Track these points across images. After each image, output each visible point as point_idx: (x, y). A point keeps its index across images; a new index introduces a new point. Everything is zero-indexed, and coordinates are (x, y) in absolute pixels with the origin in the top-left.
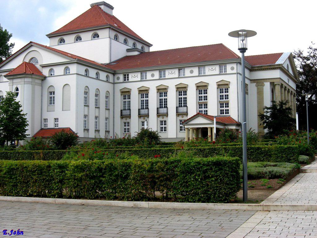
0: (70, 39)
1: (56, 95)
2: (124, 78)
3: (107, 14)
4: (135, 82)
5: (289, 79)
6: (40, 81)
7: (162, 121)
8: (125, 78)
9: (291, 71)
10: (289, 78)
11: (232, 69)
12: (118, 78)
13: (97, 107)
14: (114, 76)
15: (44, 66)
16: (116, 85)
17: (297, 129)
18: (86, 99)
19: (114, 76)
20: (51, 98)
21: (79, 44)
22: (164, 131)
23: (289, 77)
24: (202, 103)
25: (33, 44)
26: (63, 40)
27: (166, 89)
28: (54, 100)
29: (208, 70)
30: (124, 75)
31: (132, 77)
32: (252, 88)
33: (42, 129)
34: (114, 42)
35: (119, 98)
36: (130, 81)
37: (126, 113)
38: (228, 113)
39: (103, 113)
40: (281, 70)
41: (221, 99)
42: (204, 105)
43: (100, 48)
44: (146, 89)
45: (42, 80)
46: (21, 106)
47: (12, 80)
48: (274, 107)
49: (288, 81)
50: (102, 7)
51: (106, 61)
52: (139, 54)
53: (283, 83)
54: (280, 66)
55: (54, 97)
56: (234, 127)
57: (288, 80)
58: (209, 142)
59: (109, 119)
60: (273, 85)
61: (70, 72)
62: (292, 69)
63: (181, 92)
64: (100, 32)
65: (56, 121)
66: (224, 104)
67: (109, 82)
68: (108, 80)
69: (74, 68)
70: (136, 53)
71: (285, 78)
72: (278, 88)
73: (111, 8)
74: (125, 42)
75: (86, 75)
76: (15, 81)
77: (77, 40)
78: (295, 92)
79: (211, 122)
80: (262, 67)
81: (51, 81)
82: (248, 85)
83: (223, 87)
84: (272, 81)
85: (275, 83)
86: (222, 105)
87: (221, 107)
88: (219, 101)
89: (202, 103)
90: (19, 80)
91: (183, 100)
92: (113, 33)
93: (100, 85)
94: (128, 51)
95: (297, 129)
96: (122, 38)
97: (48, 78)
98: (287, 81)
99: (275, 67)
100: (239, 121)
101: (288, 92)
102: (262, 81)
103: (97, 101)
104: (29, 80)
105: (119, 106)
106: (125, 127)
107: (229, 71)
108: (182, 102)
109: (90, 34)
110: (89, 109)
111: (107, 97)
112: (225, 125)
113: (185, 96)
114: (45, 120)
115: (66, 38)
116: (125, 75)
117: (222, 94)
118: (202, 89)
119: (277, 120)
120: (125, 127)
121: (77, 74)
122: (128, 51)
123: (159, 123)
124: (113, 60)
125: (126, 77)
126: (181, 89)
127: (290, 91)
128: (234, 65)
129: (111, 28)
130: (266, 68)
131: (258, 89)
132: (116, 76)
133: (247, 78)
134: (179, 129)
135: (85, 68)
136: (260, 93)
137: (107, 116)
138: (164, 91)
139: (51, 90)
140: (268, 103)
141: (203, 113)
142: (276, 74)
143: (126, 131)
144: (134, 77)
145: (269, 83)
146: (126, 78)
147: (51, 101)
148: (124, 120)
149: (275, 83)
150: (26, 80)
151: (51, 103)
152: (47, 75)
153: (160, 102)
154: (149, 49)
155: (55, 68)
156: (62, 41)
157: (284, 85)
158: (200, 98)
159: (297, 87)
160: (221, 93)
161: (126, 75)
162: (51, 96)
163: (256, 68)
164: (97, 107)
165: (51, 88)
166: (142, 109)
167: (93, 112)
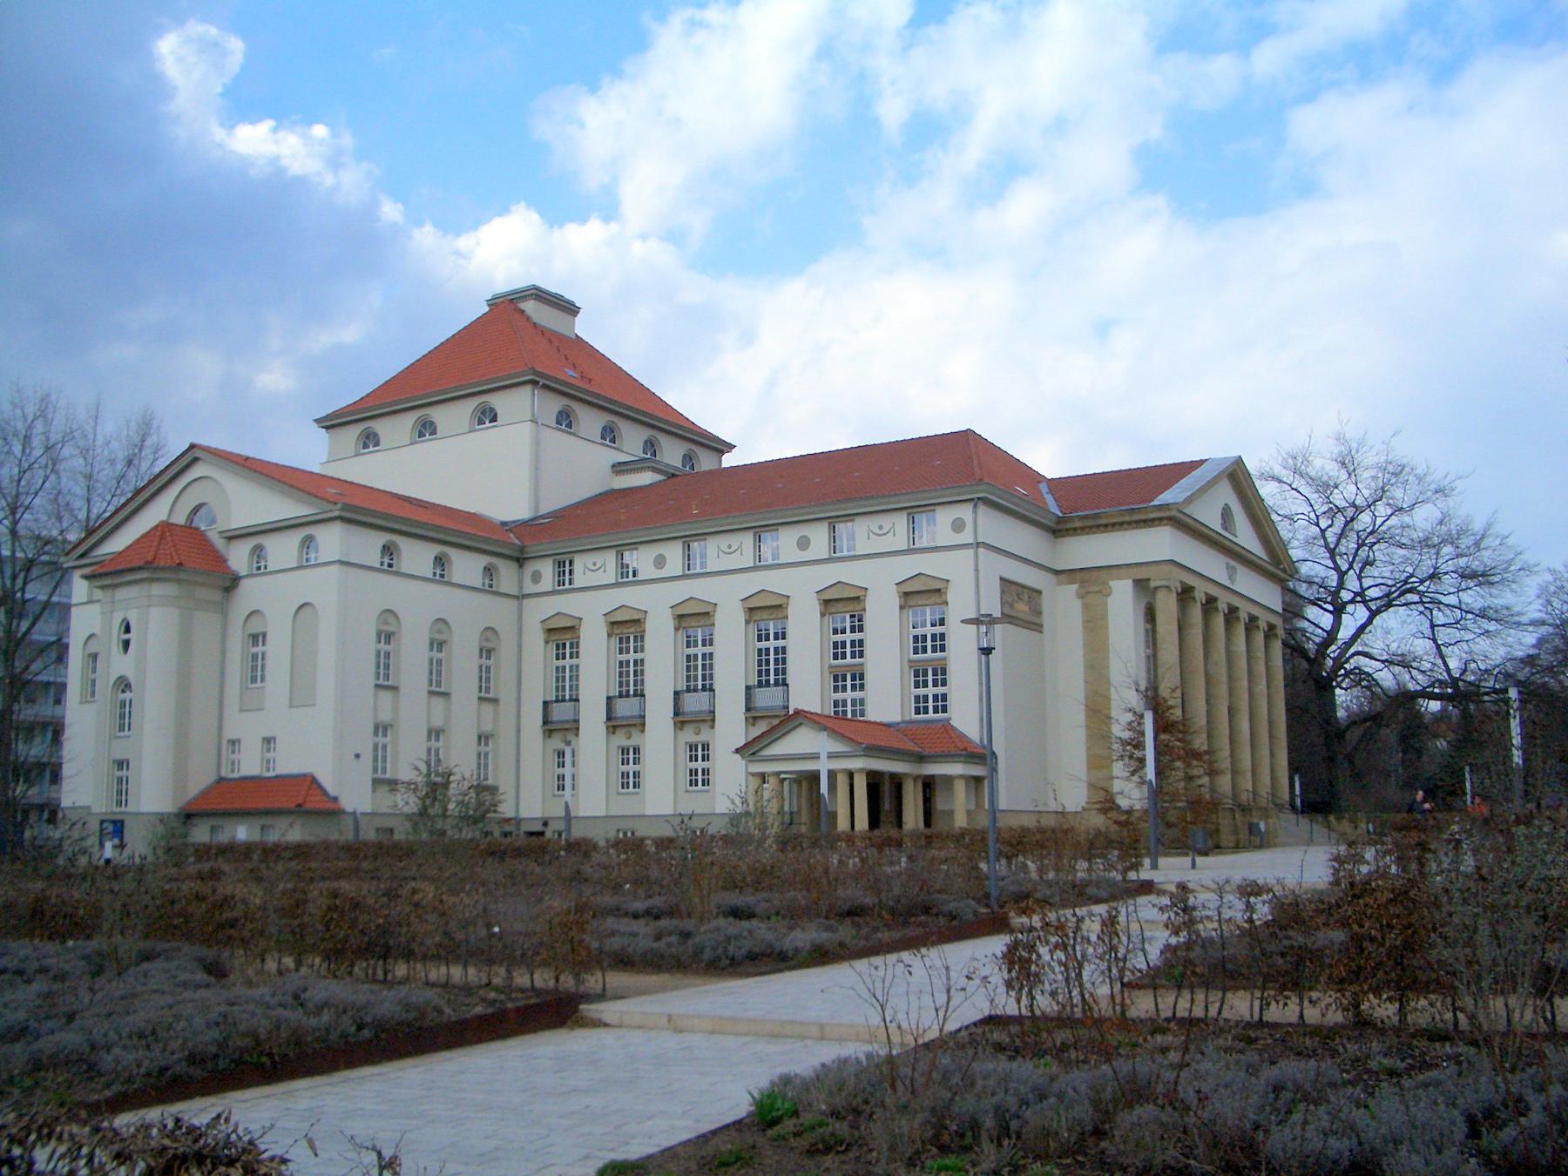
0: (396, 429)
3: (542, 331)
6: (216, 595)
10: (1232, 563)
12: (536, 578)
13: (438, 693)
14: (521, 566)
15: (233, 537)
16: (525, 602)
17: (1517, 757)
19: (521, 566)
21: (429, 447)
25: (197, 453)
26: (376, 435)
27: (707, 614)
29: (784, 543)
33: (221, 780)
35: (537, 649)
36: (577, 585)
37: (561, 712)
38: (944, 710)
41: (835, 658)
43: (496, 464)
44: (569, 624)
47: (109, 592)
49: (1231, 578)
50: (529, 307)
53: (1191, 581)
54: (1168, 514)
64: (499, 401)
65: (625, 762)
66: (928, 669)
69: (332, 540)
70: (646, 478)
72: (1167, 606)
73: (571, 309)
74: (609, 435)
77: (421, 435)
80: (1096, 516)
81: (252, 593)
82: (1039, 592)
84: (1142, 574)
85: (1153, 584)
88: (910, 661)
91: (772, 657)
92: (555, 404)
95: (1517, 757)
96: (590, 421)
97: (245, 584)
99: (1152, 516)
102: (1104, 573)
103: (436, 670)
104: (170, 589)
105: (537, 689)
108: (771, 668)
109: (467, 408)
111: (487, 652)
112: (921, 759)
114: (233, 742)
115: (381, 427)
116: (561, 564)
121: (341, 563)
123: (684, 753)
124: (545, 510)
125: (564, 568)
128: (965, 512)
131: (1086, 607)
132: (531, 567)
133: (51, 596)
134: (616, 780)
135: (382, 538)
136: (1095, 625)
139: (254, 626)
142: (1157, 544)
144: (594, 568)
145: (1129, 583)
148: (689, 735)
150: (157, 589)
152: (243, 572)
156: (370, 440)
158: (838, 650)
163: (1077, 524)
164: (438, 693)
165: (254, 619)
166: (760, 685)
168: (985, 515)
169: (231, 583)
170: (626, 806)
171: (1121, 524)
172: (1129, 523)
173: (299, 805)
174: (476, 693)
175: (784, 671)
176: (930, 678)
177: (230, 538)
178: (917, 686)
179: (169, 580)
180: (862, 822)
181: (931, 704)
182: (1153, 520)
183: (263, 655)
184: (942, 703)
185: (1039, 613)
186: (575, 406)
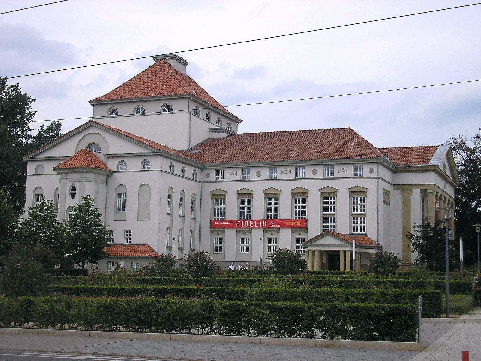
1: (128, 199)
2: (217, 175)
4: (232, 183)
5: (446, 183)
6: (104, 178)
7: (271, 238)
8: (217, 175)
9: (448, 173)
10: (445, 182)
11: (371, 171)
12: (208, 175)
14: (202, 171)
18: (170, 205)
20: (119, 201)
21: (141, 118)
22: (246, 252)
23: (446, 181)
24: (328, 216)
28: (124, 205)
30: (217, 171)
31: (228, 175)
32: (396, 196)
34: (194, 118)
35: (208, 202)
38: (364, 231)
39: (188, 225)
40: (435, 172)
42: (331, 218)
43: (178, 129)
45: (108, 176)
46: (101, 215)
47: (65, 175)
48: (425, 226)
50: (173, 62)
51: (184, 147)
52: (228, 137)
53: (438, 190)
54: (435, 168)
55: (125, 201)
56: (373, 251)
57: (445, 184)
58: (311, 273)
59: (194, 232)
60: (424, 194)
61: (151, 166)
62: (449, 167)
63: (299, 199)
65: (127, 235)
66: (358, 218)
67: (185, 177)
68: (194, 177)
70: (224, 135)
71: (440, 183)
73: (184, 63)
75: (171, 173)
76: (70, 176)
78: (453, 201)
79: (343, 243)
81: (120, 178)
83: (358, 196)
84: (424, 188)
85: (428, 191)
86: (355, 219)
87: (354, 222)
89: (328, 216)
90: (77, 176)
91: (301, 210)
92: (193, 106)
93: (184, 182)
94: (212, 131)
96: (203, 112)
97: (117, 175)
98: (442, 187)
99: (429, 169)
100: (380, 243)
101: (445, 201)
104: (92, 176)
106: (216, 245)
107: (366, 173)
110: (172, 219)
113: (304, 205)
116: (217, 171)
117: (356, 204)
118: (328, 196)
119: (431, 244)
120: (216, 245)
122: (212, 131)
125: (219, 174)
126: (299, 196)
127: (447, 200)
128: (374, 167)
129: (190, 98)
130: (416, 169)
132: (205, 172)
135: (170, 161)
137: (169, 225)
138: (274, 196)
139: (121, 190)
140: (417, 218)
141: (329, 230)
142: (430, 179)
143: (217, 250)
146: (219, 175)
147: (119, 205)
149: (428, 191)
150: (88, 175)
151: (119, 209)
152: (115, 170)
153: (268, 212)
154: (237, 126)
155: (128, 161)
156: (114, 112)
157: (440, 192)
159: (456, 191)
160: (354, 202)
161: (219, 171)
162: (120, 198)
165: (121, 187)
167: (177, 223)
168: (381, 168)
169: (110, 173)
170: (244, 258)
171: (417, 170)
172: (420, 170)
173: (151, 255)
174: (191, 217)
175: (305, 215)
176: (359, 220)
177: (108, 157)
178: (242, 204)
179: (93, 172)
180: (348, 268)
181: (359, 229)
182: (429, 170)
183: (125, 200)
184: (363, 228)
185: (389, 199)
186: (200, 107)
